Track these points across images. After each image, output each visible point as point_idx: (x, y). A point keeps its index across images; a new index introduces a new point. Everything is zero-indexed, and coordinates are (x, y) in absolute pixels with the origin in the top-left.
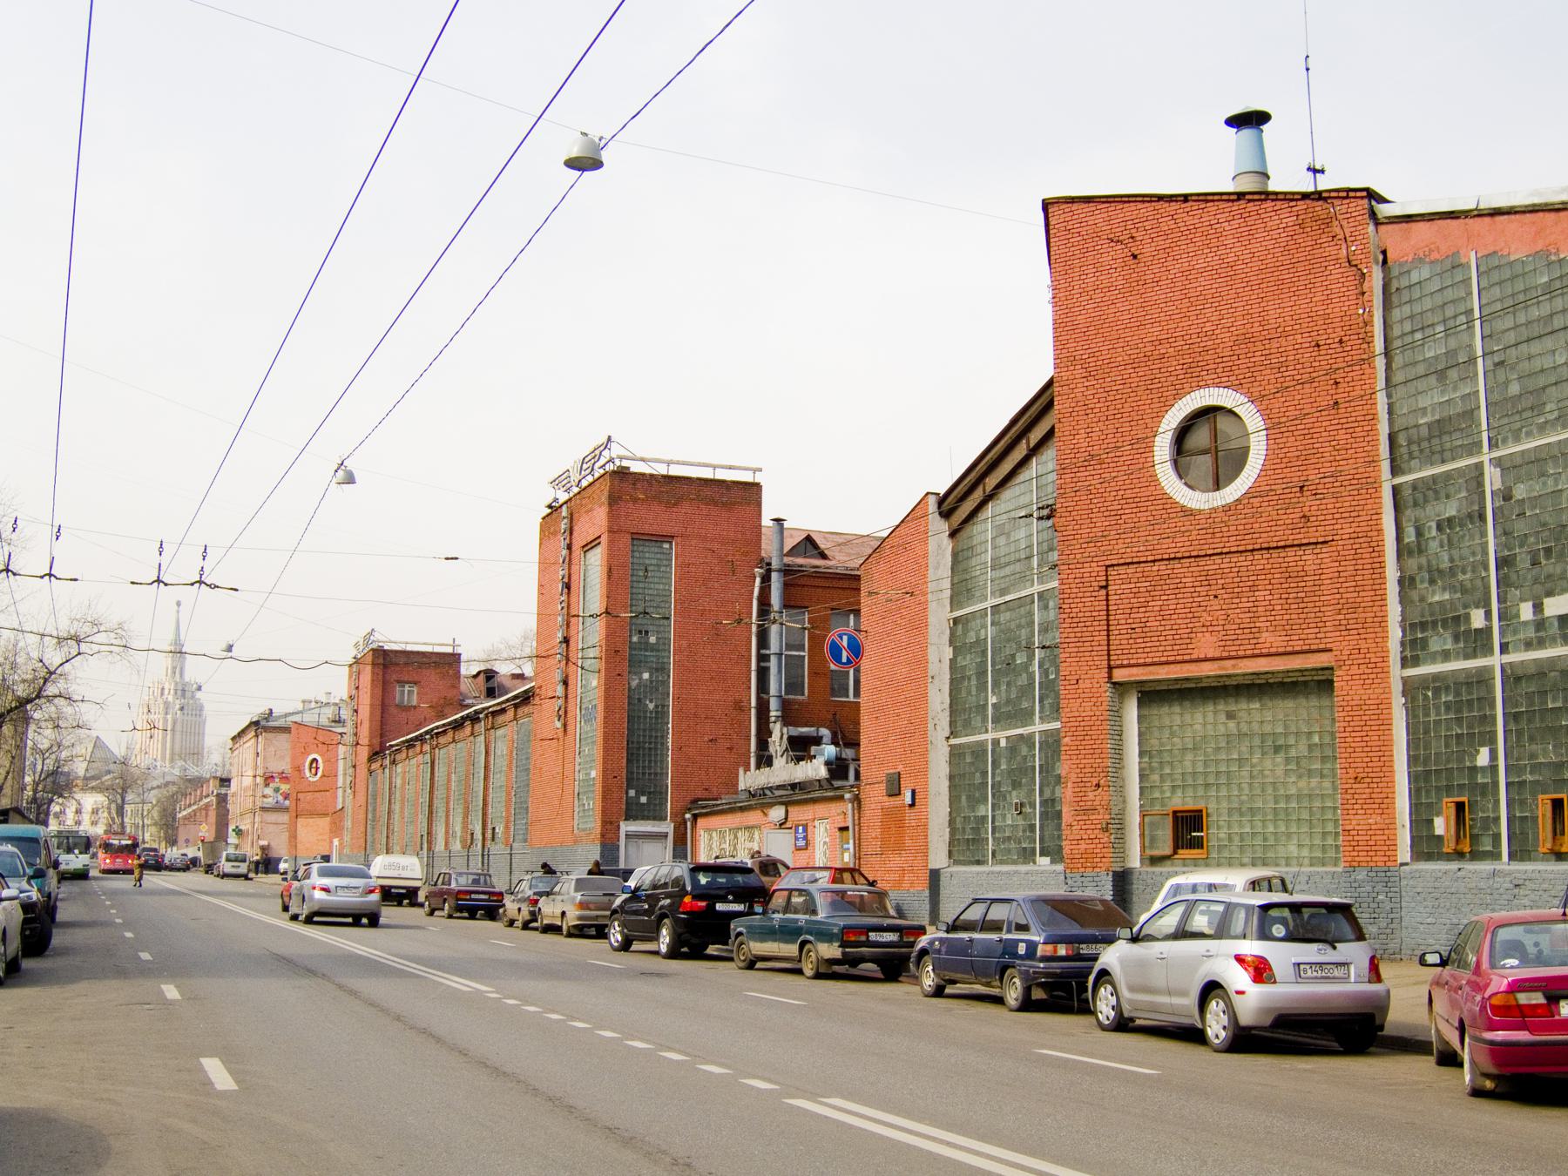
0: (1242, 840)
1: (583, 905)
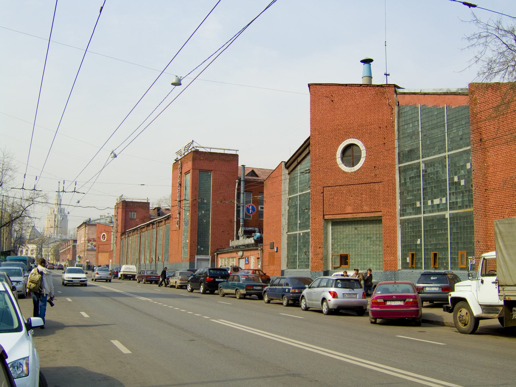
0: (358, 263)
1: (181, 280)
